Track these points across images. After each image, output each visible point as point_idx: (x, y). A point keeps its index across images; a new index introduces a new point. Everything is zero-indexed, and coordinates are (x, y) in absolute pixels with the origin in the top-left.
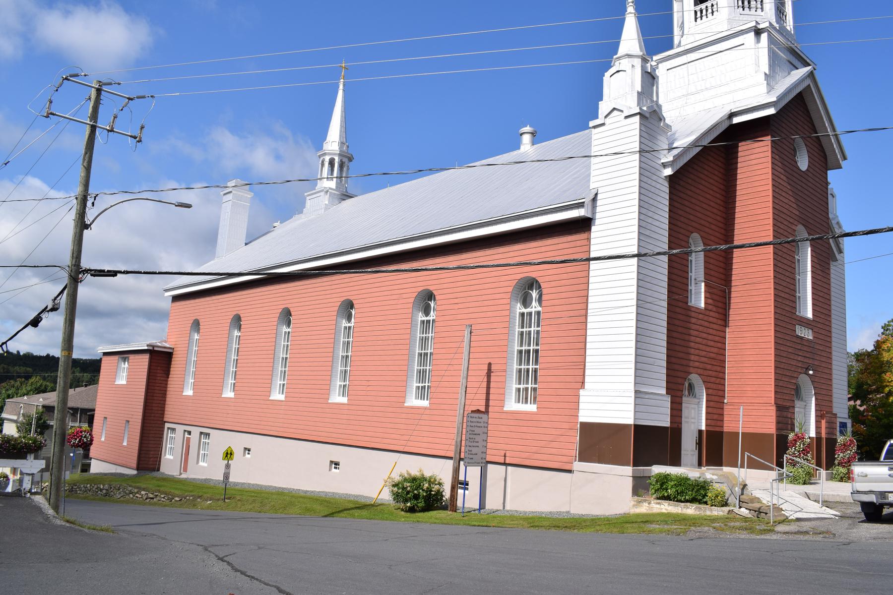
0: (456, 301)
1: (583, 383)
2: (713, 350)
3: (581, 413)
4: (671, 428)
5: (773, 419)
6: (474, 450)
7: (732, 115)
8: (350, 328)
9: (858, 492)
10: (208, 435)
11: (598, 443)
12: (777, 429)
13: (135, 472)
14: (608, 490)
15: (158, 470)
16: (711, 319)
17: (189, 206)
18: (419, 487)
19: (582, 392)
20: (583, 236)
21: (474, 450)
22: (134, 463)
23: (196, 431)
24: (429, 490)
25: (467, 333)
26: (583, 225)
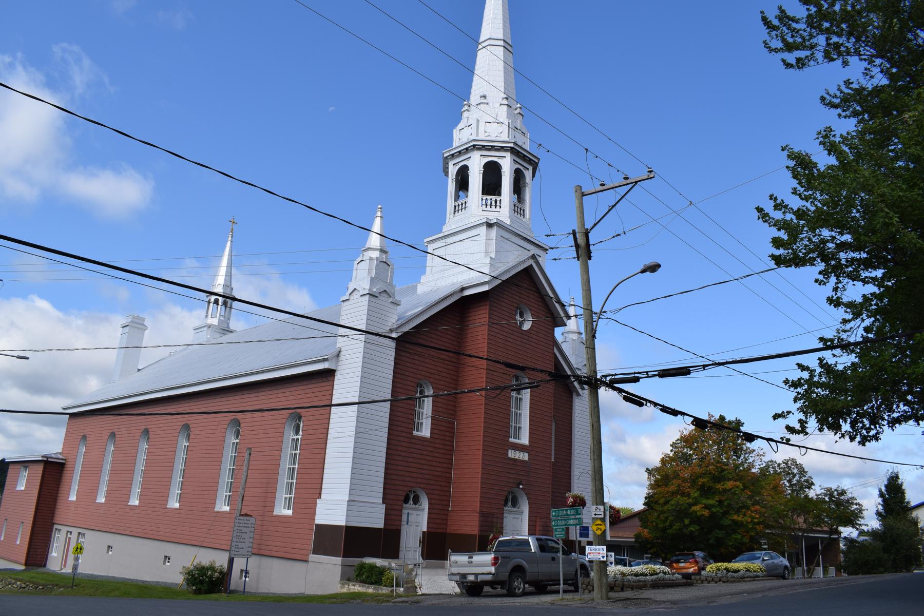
0: (252, 428)
1: (320, 494)
2: (438, 469)
3: (317, 517)
4: (385, 529)
5: (477, 523)
6: (241, 545)
7: (463, 289)
8: (297, 439)
9: (453, 574)
10: (84, 534)
11: (330, 540)
12: (481, 531)
13: (23, 567)
14: (325, 575)
15: (45, 566)
16: (437, 445)
17: (27, 358)
18: (205, 574)
19: (318, 501)
20: (330, 383)
21: (241, 545)
22: (23, 559)
23: (75, 531)
24: (211, 576)
25: (247, 455)
26: (329, 374)
